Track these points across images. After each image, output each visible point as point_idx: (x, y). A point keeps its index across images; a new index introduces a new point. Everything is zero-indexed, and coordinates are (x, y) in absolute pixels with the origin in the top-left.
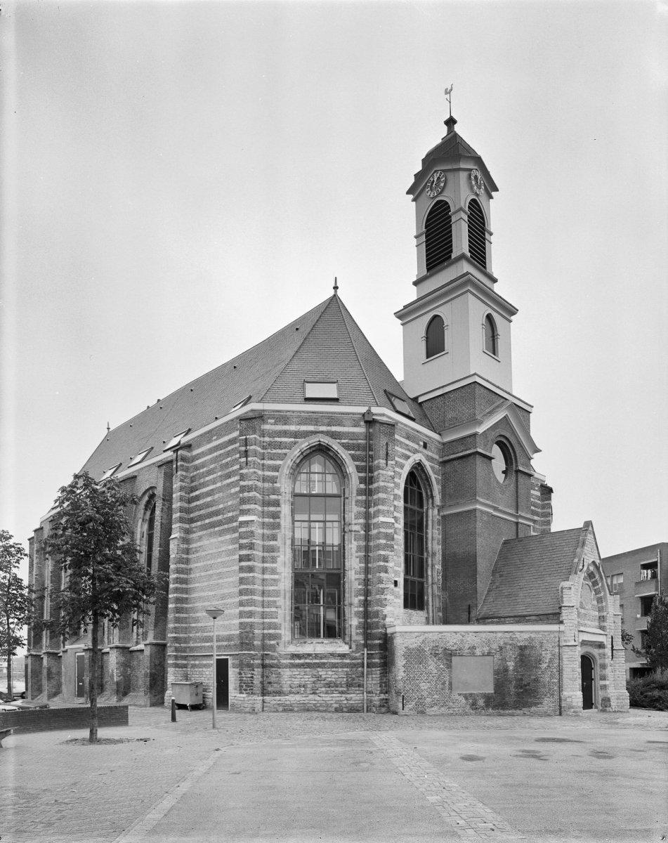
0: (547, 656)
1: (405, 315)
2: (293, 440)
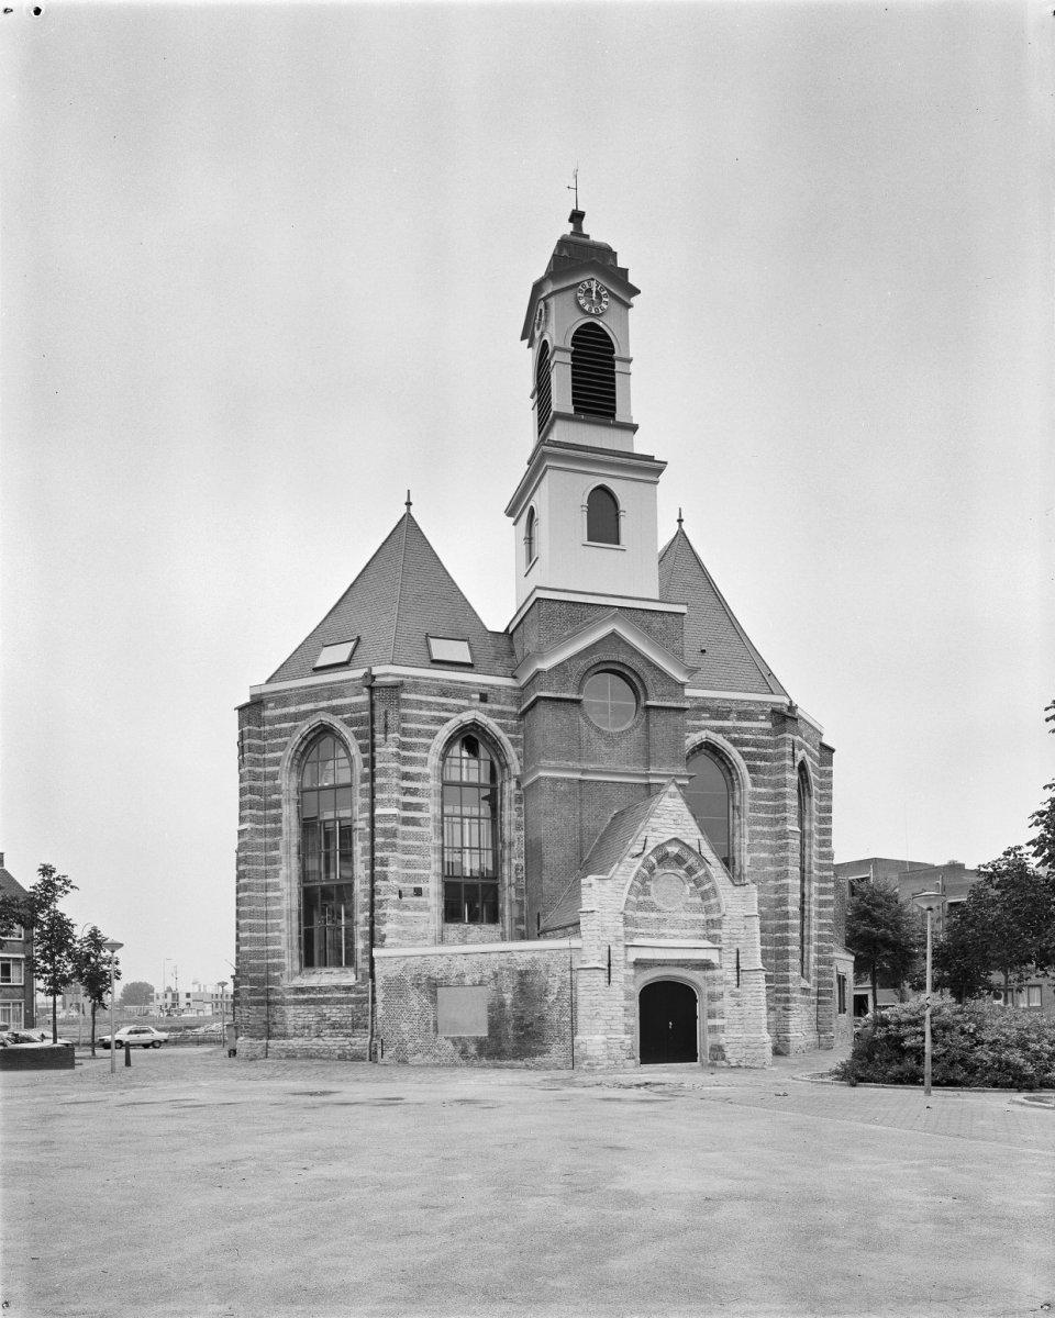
0: (555, 985)
2: (292, 724)
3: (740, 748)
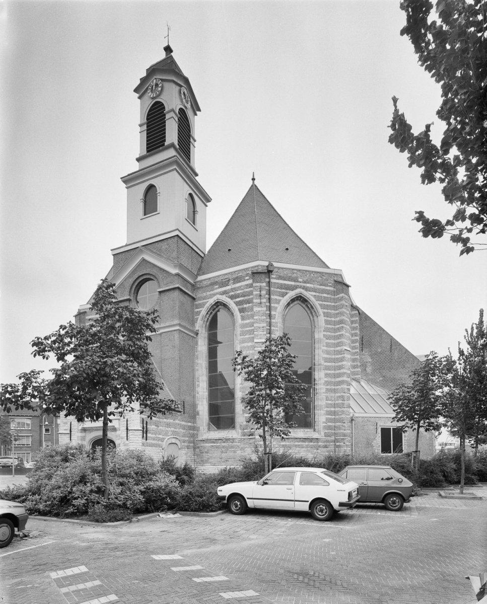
1: (129, 180)
3: (234, 300)
